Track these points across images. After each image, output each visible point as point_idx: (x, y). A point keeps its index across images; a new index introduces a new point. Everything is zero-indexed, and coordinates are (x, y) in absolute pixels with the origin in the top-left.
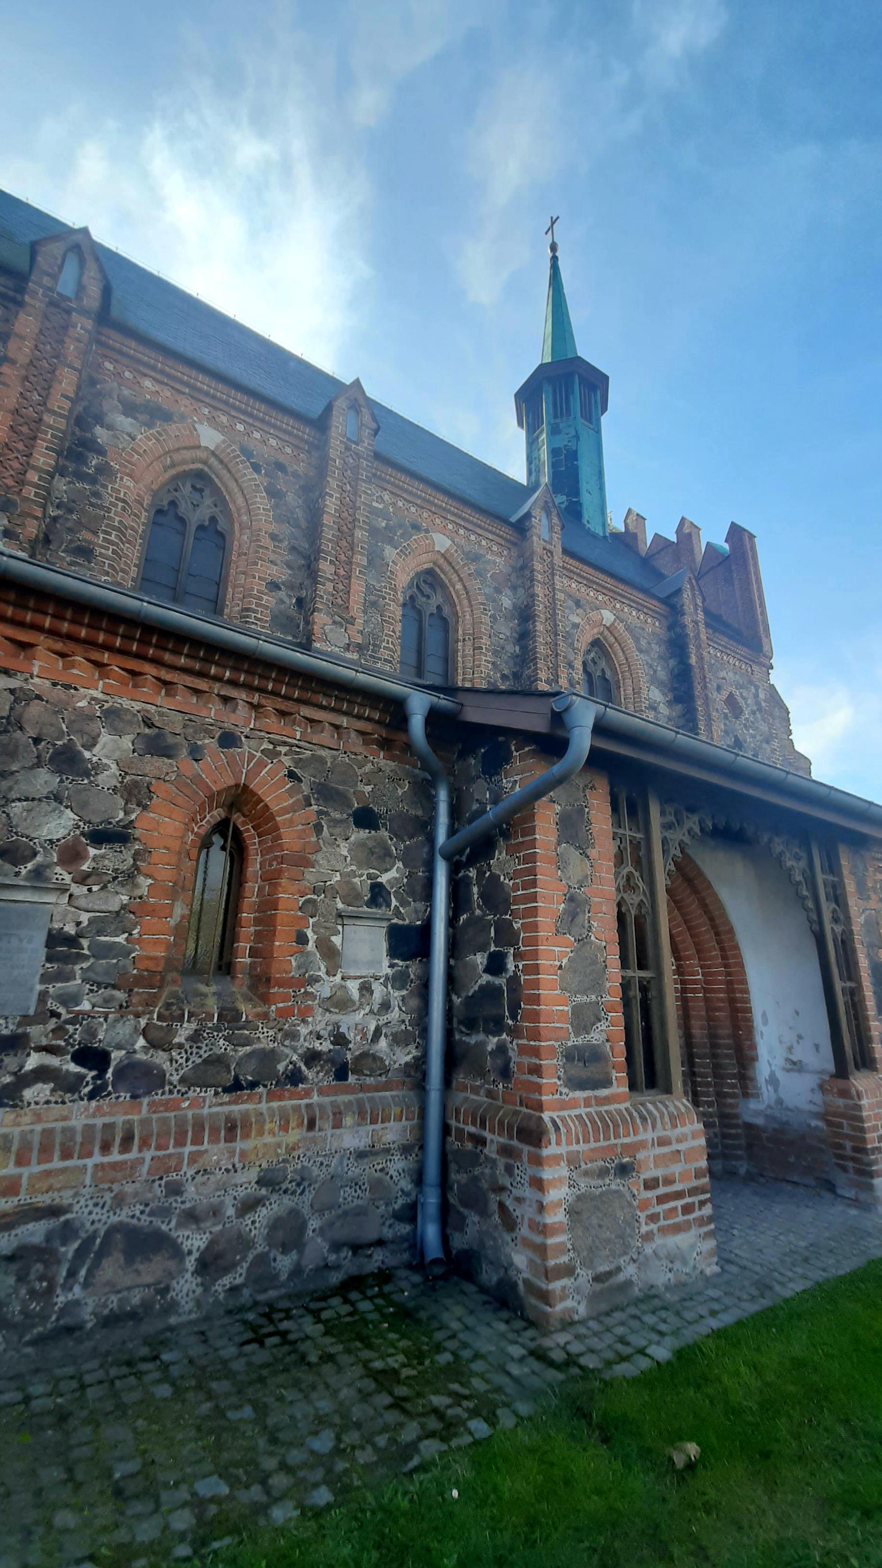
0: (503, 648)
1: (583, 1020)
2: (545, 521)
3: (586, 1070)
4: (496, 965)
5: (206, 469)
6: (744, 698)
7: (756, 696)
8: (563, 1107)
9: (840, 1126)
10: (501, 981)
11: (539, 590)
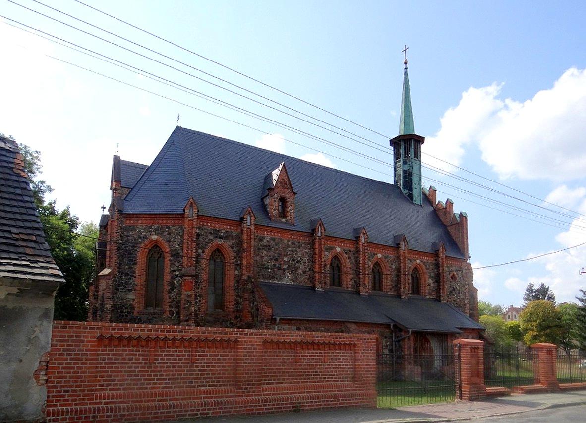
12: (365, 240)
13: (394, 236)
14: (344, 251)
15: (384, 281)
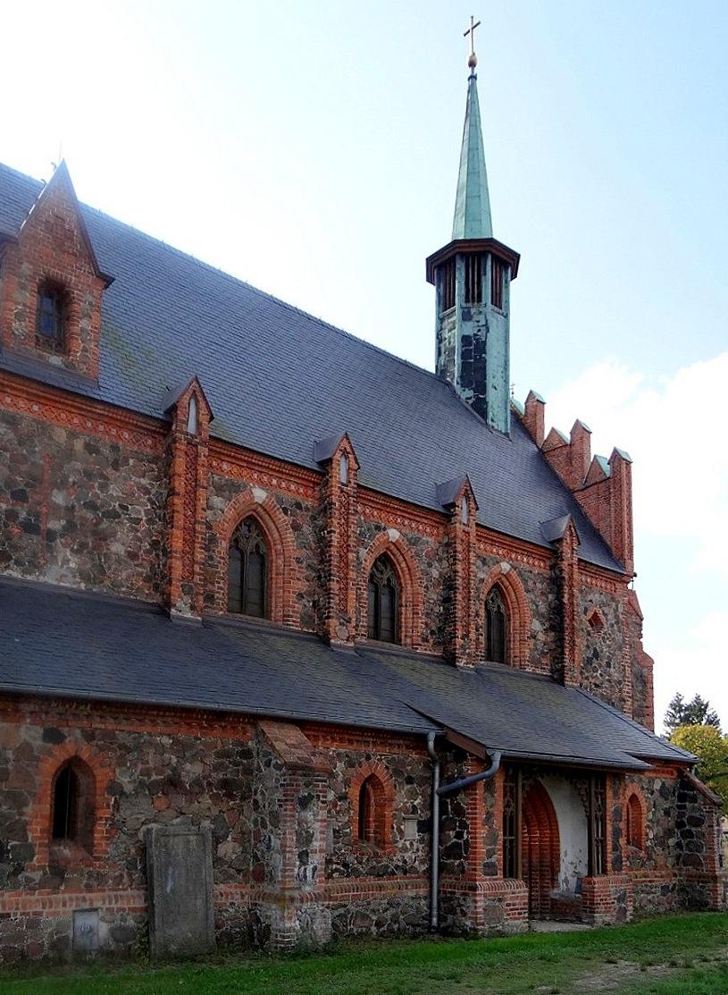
0: (432, 610)
1: (490, 854)
2: (465, 507)
3: (490, 869)
4: (459, 835)
5: (254, 514)
6: (605, 615)
7: (616, 610)
8: (483, 883)
9: (586, 895)
10: (461, 841)
11: (459, 567)
12: (348, 474)
13: (438, 487)
14: (280, 501)
15: (406, 613)
